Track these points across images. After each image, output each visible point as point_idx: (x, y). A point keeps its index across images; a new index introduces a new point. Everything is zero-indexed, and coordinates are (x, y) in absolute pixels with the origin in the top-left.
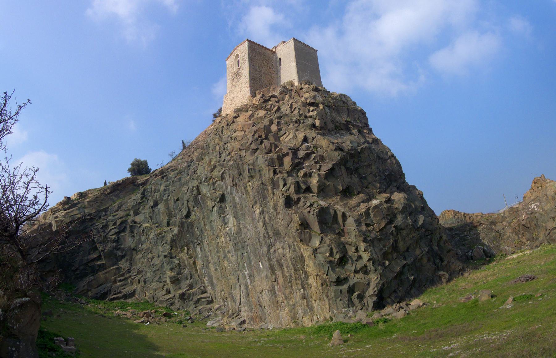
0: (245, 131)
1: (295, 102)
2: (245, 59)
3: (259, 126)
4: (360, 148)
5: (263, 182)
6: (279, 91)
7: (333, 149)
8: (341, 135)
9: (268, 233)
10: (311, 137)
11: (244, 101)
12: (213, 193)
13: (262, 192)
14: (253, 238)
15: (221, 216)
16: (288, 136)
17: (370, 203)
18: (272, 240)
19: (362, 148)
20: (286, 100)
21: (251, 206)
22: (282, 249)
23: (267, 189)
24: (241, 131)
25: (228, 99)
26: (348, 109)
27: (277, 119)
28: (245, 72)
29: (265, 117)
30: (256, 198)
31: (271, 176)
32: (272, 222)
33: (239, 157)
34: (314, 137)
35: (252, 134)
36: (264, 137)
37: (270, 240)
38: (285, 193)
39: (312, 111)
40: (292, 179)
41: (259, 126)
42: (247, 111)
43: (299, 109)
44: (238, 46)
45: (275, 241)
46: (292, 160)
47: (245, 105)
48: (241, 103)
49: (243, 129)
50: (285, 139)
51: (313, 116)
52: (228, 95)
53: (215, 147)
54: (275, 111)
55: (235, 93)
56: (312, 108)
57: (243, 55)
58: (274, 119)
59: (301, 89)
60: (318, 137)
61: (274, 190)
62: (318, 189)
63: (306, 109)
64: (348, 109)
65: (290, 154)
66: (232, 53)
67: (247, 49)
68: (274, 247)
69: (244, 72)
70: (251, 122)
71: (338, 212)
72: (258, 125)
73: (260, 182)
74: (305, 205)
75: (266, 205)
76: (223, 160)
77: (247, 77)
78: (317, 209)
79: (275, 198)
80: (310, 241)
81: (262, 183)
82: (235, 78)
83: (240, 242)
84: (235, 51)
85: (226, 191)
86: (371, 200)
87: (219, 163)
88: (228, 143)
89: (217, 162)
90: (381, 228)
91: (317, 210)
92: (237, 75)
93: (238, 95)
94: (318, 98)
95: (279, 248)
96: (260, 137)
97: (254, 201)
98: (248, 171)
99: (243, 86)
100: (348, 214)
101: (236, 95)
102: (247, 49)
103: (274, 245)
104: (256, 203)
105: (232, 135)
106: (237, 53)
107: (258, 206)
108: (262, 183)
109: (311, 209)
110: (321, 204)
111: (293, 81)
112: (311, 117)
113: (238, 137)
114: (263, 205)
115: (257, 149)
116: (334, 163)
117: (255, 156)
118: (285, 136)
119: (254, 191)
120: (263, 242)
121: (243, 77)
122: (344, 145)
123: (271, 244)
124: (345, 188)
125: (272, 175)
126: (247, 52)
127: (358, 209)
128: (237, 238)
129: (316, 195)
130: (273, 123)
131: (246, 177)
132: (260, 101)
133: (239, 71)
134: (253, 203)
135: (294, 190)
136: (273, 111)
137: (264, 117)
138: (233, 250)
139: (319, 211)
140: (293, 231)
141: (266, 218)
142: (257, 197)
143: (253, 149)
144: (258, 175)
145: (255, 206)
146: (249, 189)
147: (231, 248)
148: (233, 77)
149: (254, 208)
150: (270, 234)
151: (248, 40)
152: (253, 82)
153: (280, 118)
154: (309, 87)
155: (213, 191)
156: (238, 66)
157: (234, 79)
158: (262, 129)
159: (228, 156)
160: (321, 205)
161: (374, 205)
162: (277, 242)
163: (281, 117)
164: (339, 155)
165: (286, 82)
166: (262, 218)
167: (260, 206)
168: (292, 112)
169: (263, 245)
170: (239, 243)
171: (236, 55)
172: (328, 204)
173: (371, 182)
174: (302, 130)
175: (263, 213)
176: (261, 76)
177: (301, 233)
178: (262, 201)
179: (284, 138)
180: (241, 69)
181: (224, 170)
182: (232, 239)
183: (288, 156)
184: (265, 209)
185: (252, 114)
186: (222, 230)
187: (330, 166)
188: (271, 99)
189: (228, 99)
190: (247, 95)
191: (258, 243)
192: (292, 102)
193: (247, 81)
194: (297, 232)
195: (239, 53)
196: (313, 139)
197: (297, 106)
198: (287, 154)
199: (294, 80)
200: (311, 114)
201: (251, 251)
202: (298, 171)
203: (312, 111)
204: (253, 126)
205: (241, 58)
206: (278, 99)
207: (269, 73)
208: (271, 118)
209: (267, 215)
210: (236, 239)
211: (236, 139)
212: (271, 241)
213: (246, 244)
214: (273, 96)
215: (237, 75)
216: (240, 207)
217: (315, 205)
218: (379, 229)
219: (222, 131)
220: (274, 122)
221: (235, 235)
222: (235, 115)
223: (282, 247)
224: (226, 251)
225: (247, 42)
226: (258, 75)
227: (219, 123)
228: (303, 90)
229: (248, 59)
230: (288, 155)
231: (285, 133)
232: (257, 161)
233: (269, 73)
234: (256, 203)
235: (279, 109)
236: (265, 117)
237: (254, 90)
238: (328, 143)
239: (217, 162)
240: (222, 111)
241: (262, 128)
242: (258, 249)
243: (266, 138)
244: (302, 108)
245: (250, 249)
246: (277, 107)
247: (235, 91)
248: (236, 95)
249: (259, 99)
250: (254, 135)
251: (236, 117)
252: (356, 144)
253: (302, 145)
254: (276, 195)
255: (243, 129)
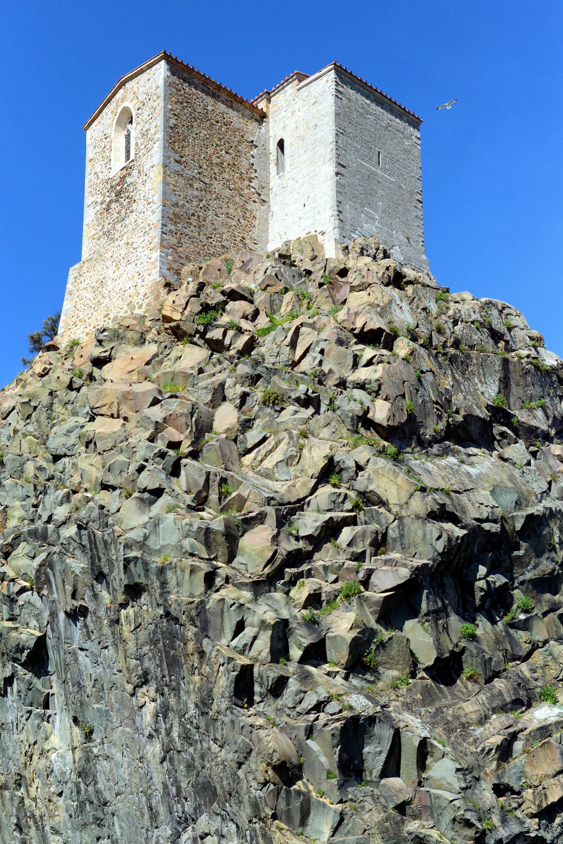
0: (126, 419)
1: (312, 326)
2: (152, 131)
3: (174, 406)
4: (524, 514)
5: (172, 610)
6: (261, 272)
7: (423, 512)
8: (462, 462)
9: (176, 783)
10: (353, 464)
11: (136, 300)
12: (11, 629)
13: (165, 646)
14: (132, 793)
15: (30, 712)
16: (270, 451)
17: (527, 716)
18: (189, 807)
19: (530, 518)
20: (282, 310)
21: (129, 687)
22: (215, 838)
23: (183, 636)
24: (112, 416)
25: (84, 285)
26: (506, 362)
27: (242, 384)
28: (148, 185)
29: (201, 371)
30: (147, 664)
31: (197, 593)
32: (191, 750)
33: (97, 511)
34: (362, 463)
35: (147, 434)
36: (185, 448)
37: (183, 806)
38: (237, 656)
39: (369, 363)
40: (267, 608)
41: (174, 406)
42: (142, 341)
43: (322, 352)
44: (131, 78)
45: (198, 810)
46: (275, 539)
47: (135, 318)
48: (125, 308)
49: (118, 411)
50: (261, 461)
51: (370, 382)
52: (85, 269)
53: (22, 465)
54: (239, 352)
55: (109, 263)
56: (368, 352)
57: (145, 117)
58: (229, 382)
59: (344, 273)
60: (376, 463)
61: (205, 641)
62: (350, 653)
63: (345, 356)
64: (506, 362)
65: (271, 520)
66: (109, 101)
67: (161, 91)
68: (193, 828)
69: (144, 183)
70: (148, 386)
71: (405, 736)
72: (174, 400)
73: (161, 611)
74: (300, 702)
75: (176, 690)
76: (45, 518)
77: (154, 206)
78: (338, 720)
79: (206, 669)
80: (303, 822)
81: (168, 614)
82: (113, 205)
83: (91, 803)
84: (118, 96)
85: (53, 630)
86: (529, 706)
87: (32, 527)
88: (65, 455)
89: (26, 522)
90: (548, 807)
91: (338, 724)
92: (118, 194)
93: (117, 273)
94: (398, 311)
95: (207, 835)
96: (174, 445)
97: (140, 672)
98: (125, 567)
99: (138, 239)
100: (440, 746)
101: (110, 272)
102: (162, 95)
103: (194, 821)
104: (145, 679)
105: (82, 427)
106: (125, 104)
107: (151, 690)
108: (168, 614)
109: (317, 719)
110: (354, 704)
111: (320, 238)
112: (362, 386)
113: (101, 438)
114: (166, 689)
115: (158, 493)
116: (418, 562)
117: (152, 514)
118: (264, 449)
119: (143, 635)
120: (162, 810)
121: (139, 206)
122: (464, 498)
123: (186, 819)
124: (447, 655)
125: (200, 587)
126: (162, 104)
127: (479, 731)
128: (82, 786)
129: (343, 672)
130: (224, 399)
131: (117, 588)
132: (188, 309)
133: (129, 180)
134: (135, 680)
135: (268, 650)
136: (232, 352)
137: (195, 372)
138: (69, 825)
139: (343, 730)
140: (254, 784)
141: (175, 734)
142: (150, 659)
143: (145, 490)
144: (157, 584)
145: (144, 689)
146: (126, 630)
147: (61, 817)
148: (108, 200)
149: (139, 694)
150: (183, 785)
151: (167, 58)
152: (173, 228)
153: (254, 379)
154: (374, 267)
155: (10, 624)
156: (128, 157)
157: (108, 209)
158: (183, 419)
159: (61, 504)
160: (351, 708)
161: (538, 726)
162: (201, 813)
163: (258, 377)
164: (439, 538)
165: (294, 238)
166: (163, 732)
167: (157, 691)
168: (295, 364)
169: (162, 817)
170: (87, 805)
171: (120, 109)
172: (378, 709)
173: (546, 642)
174: (325, 433)
175: (165, 717)
176: (206, 208)
177: (279, 793)
178: (164, 677)
179: (260, 458)
180: (135, 173)
181: (46, 554)
182: (65, 790)
183: (260, 527)
184: (172, 701)
185: (156, 355)
186: (35, 758)
187: (404, 574)
188: (228, 307)
189: (84, 285)
190: (151, 278)
191: (146, 810)
192: (302, 325)
193: (155, 221)
194: (265, 789)
195: (131, 106)
196: (359, 468)
197: (318, 342)
198: (261, 518)
199: (323, 233)
200: (363, 374)
201: (122, 835)
202: (292, 583)
203: (369, 363)
204: (155, 402)
205: (139, 127)
206: (253, 309)
207: (237, 199)
208: (220, 377)
209: (176, 723)
210: (79, 792)
211: (92, 446)
212: (186, 809)
213: (110, 809)
214: (233, 295)
215: (118, 194)
216: (94, 687)
217: (332, 707)
218: (539, 806)
219: (50, 407)
220: (229, 393)
221: (74, 776)
222: (98, 352)
223: (217, 830)
224: (47, 828)
225: (163, 62)
226: (195, 203)
227: (42, 376)
228: (351, 277)
229: (160, 135)
230: (262, 523)
231: (264, 439)
232: (157, 534)
233: (237, 199)
234: (146, 682)
235: (251, 345)
236: (201, 371)
237: (175, 261)
238: (406, 489)
239: (26, 522)
240: (60, 331)
241: (182, 415)
242: (144, 831)
243: (195, 455)
244: (334, 350)
245: (121, 827)
246: (245, 338)
247: (108, 255)
248: (110, 272)
249: (184, 302)
250: (152, 439)
251: (99, 362)
252: (509, 499)
253: (314, 489)
254: (209, 659)
255: (118, 411)
